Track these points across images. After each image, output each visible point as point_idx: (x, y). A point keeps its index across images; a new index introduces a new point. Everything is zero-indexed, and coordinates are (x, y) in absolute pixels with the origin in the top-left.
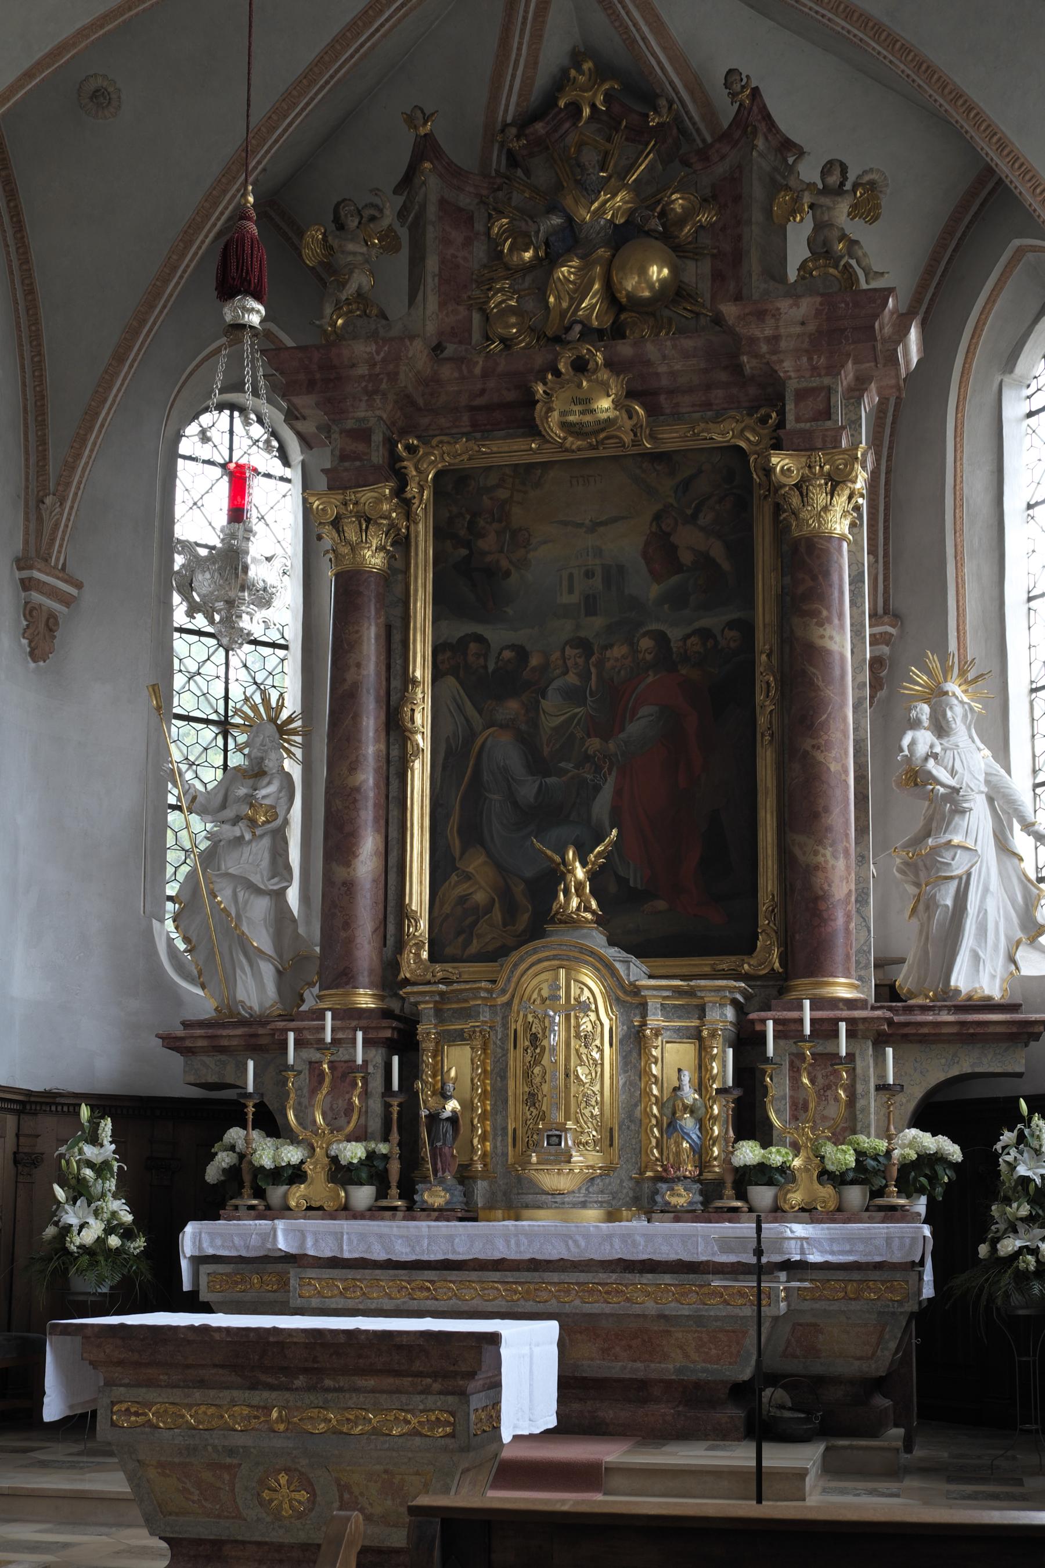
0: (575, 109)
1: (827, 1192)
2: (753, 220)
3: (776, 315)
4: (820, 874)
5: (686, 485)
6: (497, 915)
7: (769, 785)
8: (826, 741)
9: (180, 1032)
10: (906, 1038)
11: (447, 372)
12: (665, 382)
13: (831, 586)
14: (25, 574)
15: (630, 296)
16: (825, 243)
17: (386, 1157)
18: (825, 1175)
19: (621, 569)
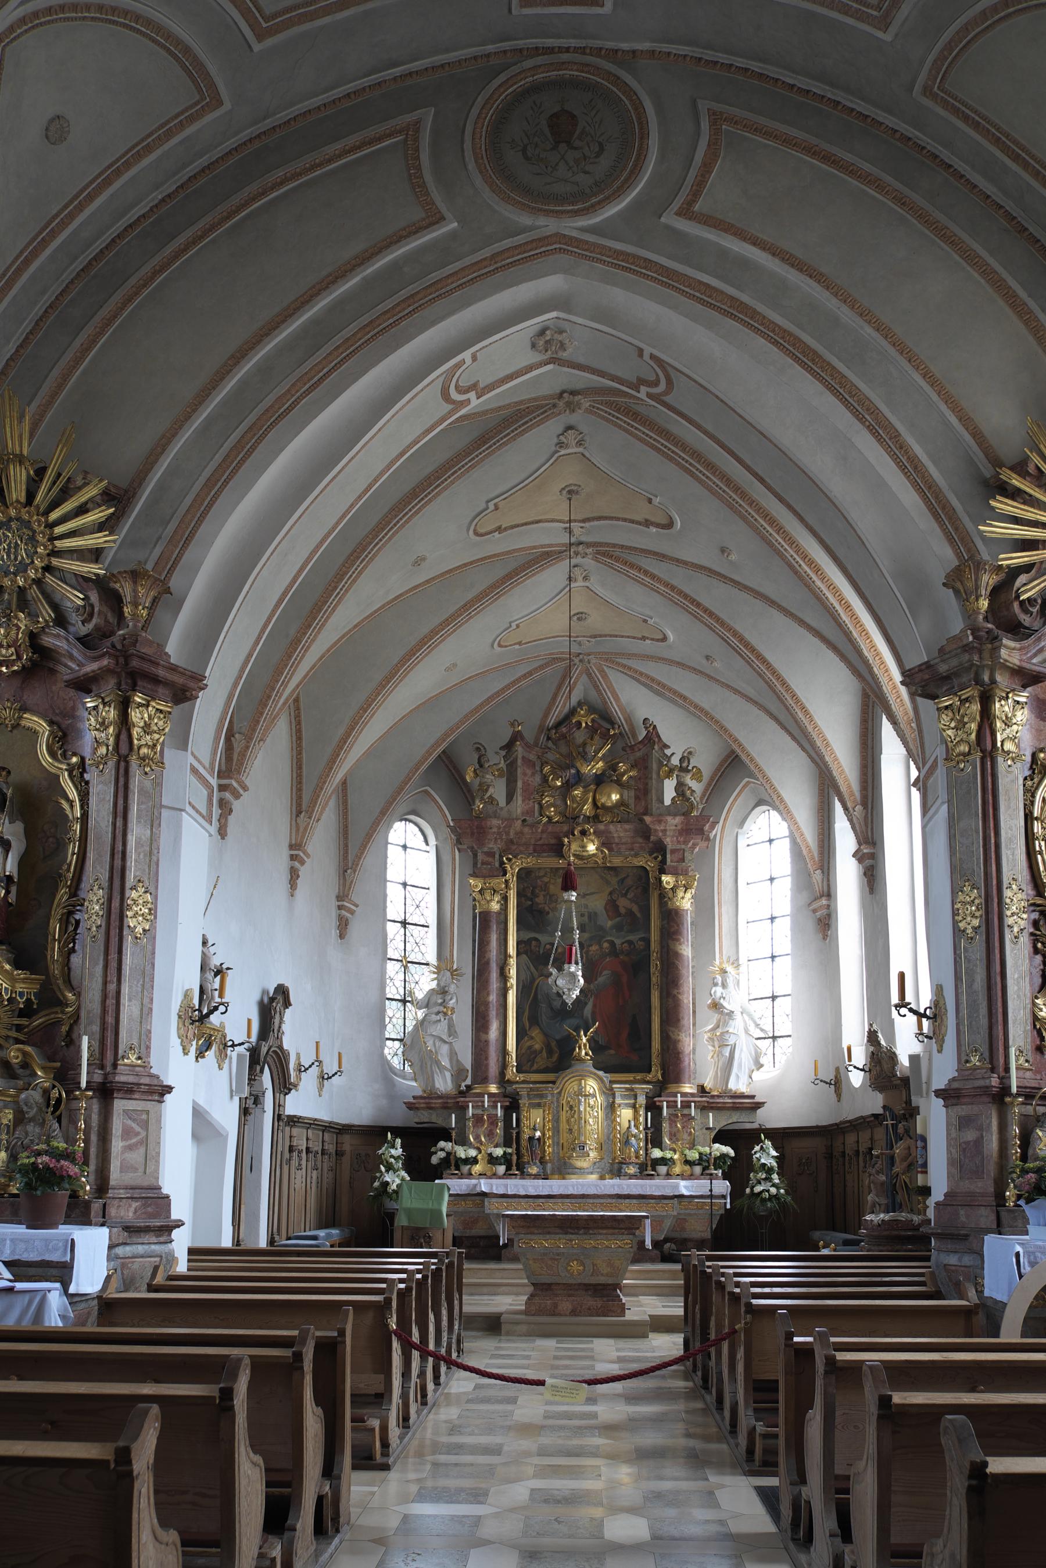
0: (579, 723)
1: (687, 1167)
3: (666, 822)
5: (622, 881)
6: (544, 1054)
9: (412, 1100)
10: (719, 1109)
12: (617, 840)
14: (340, 903)
15: (603, 805)
17: (511, 1154)
18: (687, 1162)
19: (596, 913)
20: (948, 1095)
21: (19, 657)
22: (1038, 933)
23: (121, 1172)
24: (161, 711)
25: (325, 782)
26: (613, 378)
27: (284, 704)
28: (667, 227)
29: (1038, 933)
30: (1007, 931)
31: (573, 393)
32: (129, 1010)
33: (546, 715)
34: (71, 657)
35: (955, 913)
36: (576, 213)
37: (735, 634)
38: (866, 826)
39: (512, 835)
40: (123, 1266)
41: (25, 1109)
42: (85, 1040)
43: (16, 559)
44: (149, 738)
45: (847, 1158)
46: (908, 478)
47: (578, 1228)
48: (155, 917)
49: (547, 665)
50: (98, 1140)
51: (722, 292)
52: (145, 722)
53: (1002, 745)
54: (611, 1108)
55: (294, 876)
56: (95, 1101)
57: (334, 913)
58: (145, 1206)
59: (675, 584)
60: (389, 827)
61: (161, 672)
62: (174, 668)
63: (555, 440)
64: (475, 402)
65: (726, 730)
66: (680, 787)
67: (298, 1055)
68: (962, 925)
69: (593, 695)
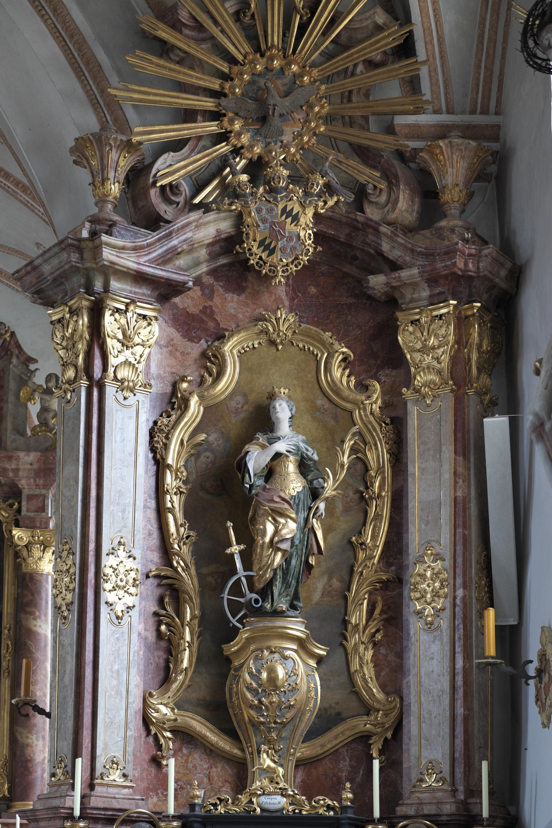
2: (9, 400)
3: (18, 459)
4: (29, 748)
7: (6, 698)
8: (35, 680)
13: (41, 599)
16: (45, 419)
22: (164, 612)
24: (144, 317)
46: (45, 22)
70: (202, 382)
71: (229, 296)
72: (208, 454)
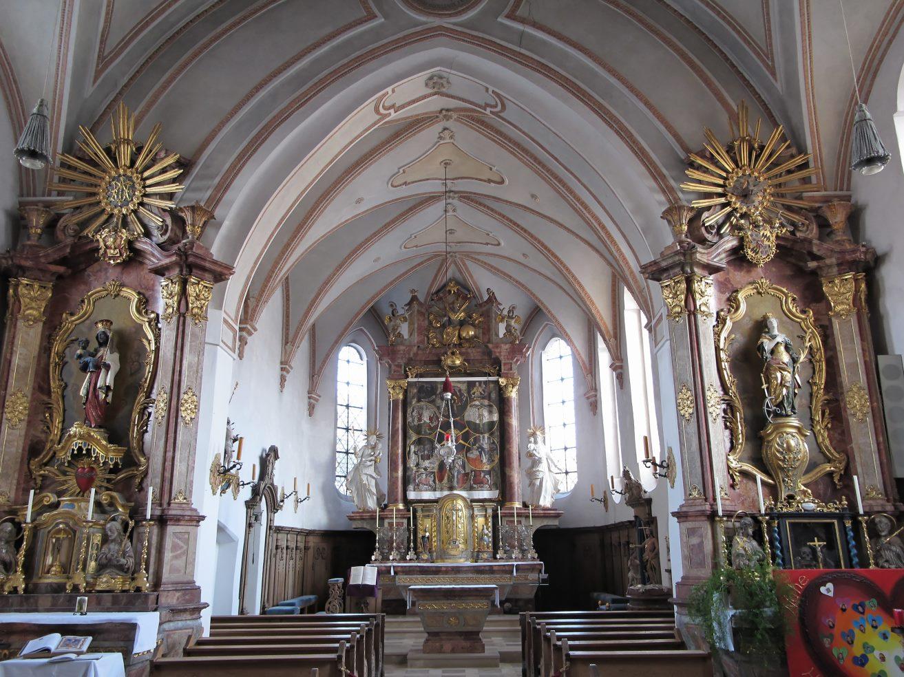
0: (450, 291)
11: (420, 352)
12: (472, 358)
14: (310, 395)
20: (681, 516)
21: (121, 255)
22: (728, 416)
23: (169, 573)
24: (206, 287)
25: (302, 325)
26: (471, 103)
27: (280, 281)
28: (501, 24)
29: (728, 416)
30: (709, 416)
31: (448, 110)
32: (180, 467)
33: (432, 285)
34: (153, 255)
35: (678, 405)
36: (450, 15)
37: (539, 242)
38: (617, 349)
39: (412, 355)
40: (168, 636)
41: (109, 533)
42: (151, 490)
43: (122, 198)
44: (198, 303)
45: (613, 547)
46: (639, 158)
47: (455, 596)
48: (199, 410)
49: (432, 258)
50: (156, 553)
51: (532, 58)
52: (197, 294)
53: (700, 308)
54: (472, 517)
55: (282, 385)
56: (155, 527)
57: (306, 401)
58: (184, 595)
59: (505, 214)
60: (339, 349)
61: (207, 265)
62: (215, 263)
63: (438, 136)
64: (393, 115)
65: (534, 295)
66: (508, 328)
67: (283, 488)
68: (682, 412)
69: (458, 275)
70: (729, 311)
71: (736, 273)
72: (737, 343)
